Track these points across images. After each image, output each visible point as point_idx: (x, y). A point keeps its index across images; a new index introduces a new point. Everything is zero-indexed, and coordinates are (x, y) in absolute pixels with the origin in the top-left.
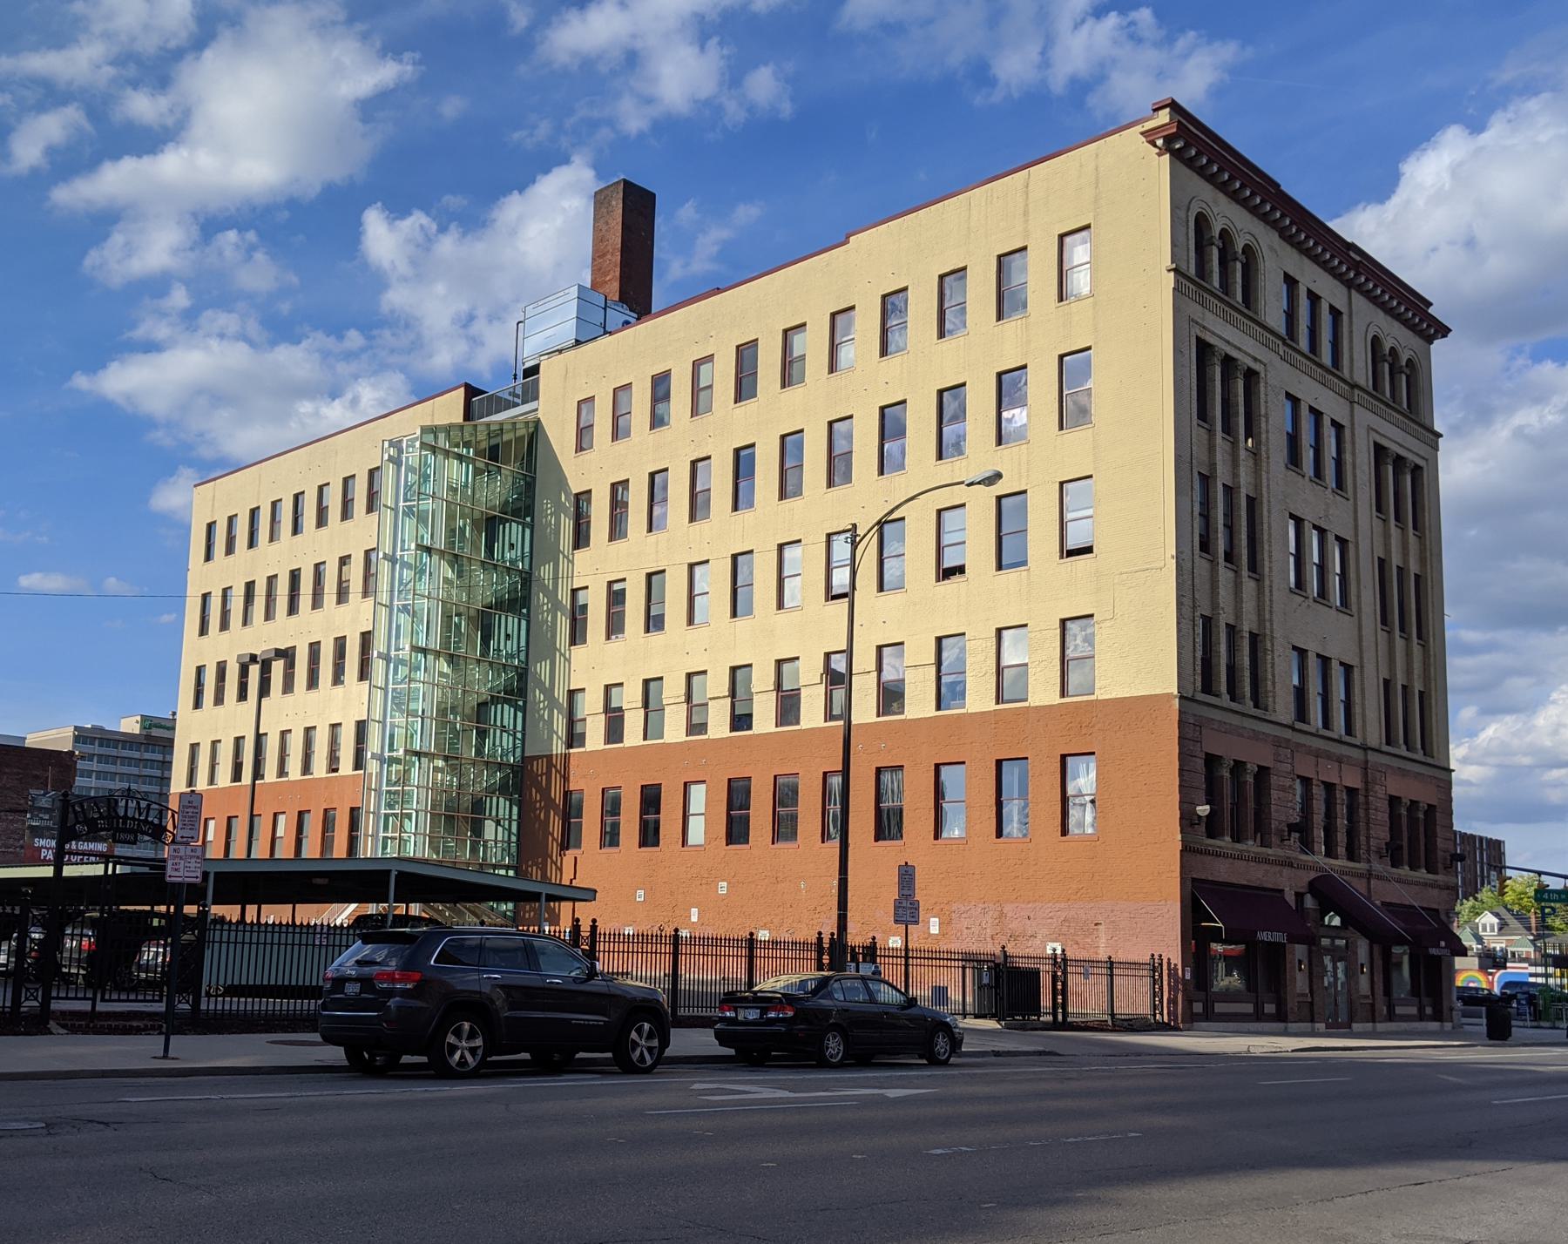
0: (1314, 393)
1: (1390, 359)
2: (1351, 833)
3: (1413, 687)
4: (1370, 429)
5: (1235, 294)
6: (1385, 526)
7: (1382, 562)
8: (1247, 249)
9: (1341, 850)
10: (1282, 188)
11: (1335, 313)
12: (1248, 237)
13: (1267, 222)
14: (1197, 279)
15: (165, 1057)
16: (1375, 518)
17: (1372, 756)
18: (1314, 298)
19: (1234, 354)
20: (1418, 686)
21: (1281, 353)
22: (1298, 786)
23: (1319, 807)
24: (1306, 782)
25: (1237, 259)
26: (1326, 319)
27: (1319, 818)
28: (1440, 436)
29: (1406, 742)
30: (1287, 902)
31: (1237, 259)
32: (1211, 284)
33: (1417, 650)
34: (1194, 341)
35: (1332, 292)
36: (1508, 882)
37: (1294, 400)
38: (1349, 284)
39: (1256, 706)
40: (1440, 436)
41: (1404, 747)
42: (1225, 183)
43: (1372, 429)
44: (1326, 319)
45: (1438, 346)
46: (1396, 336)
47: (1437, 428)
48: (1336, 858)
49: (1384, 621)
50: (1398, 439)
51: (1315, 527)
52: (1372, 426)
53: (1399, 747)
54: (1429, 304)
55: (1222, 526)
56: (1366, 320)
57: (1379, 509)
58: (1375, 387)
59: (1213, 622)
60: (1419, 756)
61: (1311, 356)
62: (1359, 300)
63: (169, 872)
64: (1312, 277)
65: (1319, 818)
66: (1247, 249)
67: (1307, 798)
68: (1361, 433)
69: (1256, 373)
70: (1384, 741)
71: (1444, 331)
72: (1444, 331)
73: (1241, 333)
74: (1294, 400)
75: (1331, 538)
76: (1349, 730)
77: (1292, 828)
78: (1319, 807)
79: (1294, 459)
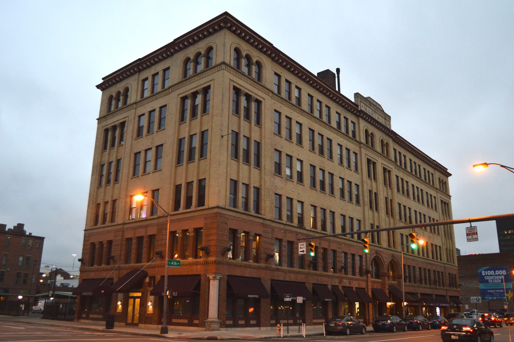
0: (401, 175)
1: (386, 145)
2: (443, 282)
3: (375, 224)
4: (440, 197)
5: (385, 153)
6: (250, 126)
7: (386, 198)
8: (372, 133)
9: (428, 283)
10: (274, 45)
11: (432, 174)
12: (372, 131)
13: (335, 102)
14: (353, 138)
15: (299, 332)
16: (368, 179)
17: (446, 265)
18: (400, 153)
19: (446, 201)
20: (451, 249)
21: (271, 96)
22: (343, 254)
23: (350, 260)
24: (346, 254)
25: (369, 136)
26: (431, 175)
27: (350, 265)
28: (451, 196)
29: (394, 246)
30: (339, 289)
31: (369, 136)
32: (369, 145)
33: (451, 242)
34: (366, 158)
35: (431, 170)
36: (103, 242)
37: (341, 146)
38: (434, 168)
39: (379, 244)
40: (451, 196)
41: (393, 248)
42: (315, 86)
43: (232, 80)
44: (431, 175)
45: (449, 178)
46: (443, 177)
47: (451, 195)
48: (427, 285)
49: (387, 214)
50: (445, 198)
51: (298, 159)
52: (231, 79)
53: (392, 248)
54: (447, 169)
55: (231, 145)
56: (437, 175)
57: (385, 184)
58: (383, 153)
59: (238, 182)
60: (377, 245)
61: (320, 119)
62: (436, 172)
63: (297, 301)
64: (399, 149)
65: (350, 265)
66: (372, 133)
67: (346, 258)
68: (439, 197)
69: (390, 171)
70: (388, 246)
71: (450, 175)
72: (450, 175)
73: (247, 84)
74: (341, 146)
75: (294, 160)
76: (441, 260)
77: (342, 267)
78: (350, 260)
79: (398, 190)
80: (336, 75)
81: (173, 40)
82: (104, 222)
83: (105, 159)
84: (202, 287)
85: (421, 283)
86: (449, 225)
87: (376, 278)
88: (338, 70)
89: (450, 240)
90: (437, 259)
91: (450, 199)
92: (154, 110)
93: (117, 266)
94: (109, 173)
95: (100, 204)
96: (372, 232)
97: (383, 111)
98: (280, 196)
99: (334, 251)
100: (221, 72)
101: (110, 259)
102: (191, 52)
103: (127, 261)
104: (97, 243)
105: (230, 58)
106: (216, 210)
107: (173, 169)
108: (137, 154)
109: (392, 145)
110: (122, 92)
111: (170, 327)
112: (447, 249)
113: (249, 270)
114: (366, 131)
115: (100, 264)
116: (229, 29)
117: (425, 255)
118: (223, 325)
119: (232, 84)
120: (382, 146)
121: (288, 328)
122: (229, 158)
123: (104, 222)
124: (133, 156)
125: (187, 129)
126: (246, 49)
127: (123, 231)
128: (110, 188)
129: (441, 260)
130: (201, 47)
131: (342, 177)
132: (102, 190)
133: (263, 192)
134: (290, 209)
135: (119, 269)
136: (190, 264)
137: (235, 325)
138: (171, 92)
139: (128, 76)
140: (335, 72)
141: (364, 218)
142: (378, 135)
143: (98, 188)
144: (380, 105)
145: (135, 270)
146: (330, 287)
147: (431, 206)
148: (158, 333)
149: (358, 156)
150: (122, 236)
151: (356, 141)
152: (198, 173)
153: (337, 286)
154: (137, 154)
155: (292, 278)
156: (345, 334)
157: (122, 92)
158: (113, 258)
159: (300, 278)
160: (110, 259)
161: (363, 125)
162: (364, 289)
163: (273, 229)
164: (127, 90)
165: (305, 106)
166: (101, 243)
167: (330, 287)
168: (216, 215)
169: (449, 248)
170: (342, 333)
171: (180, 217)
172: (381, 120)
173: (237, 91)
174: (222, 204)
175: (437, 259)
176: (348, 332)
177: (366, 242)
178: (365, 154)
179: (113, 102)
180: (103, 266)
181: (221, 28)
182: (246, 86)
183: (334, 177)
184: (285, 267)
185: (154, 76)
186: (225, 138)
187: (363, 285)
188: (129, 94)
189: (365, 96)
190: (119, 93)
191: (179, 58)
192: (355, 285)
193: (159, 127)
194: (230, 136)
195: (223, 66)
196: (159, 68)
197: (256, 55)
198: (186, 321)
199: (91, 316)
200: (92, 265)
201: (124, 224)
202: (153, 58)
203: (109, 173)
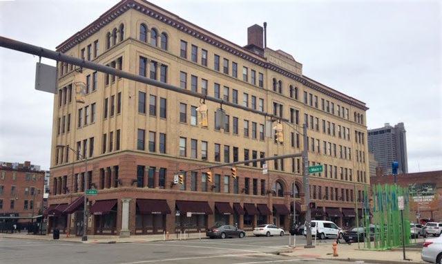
0: (310, 113)
45: (367, 111)
58: (291, 97)
76: (351, 180)
81: (98, 17)
82: (111, 150)
83: (61, 114)
84: (119, 207)
85: (343, 200)
86: (296, 158)
87: (279, 196)
88: (265, 24)
90: (346, 179)
92: (89, 75)
93: (70, 194)
94: (113, 107)
96: (276, 160)
97: (294, 61)
98: (256, 123)
99: (336, 167)
100: (128, 46)
101: (66, 190)
102: (110, 28)
103: (76, 190)
104: (105, 169)
105: (137, 34)
106: (126, 153)
108: (80, 110)
109: (301, 88)
110: (118, 28)
111: (88, 236)
112: (358, 171)
113: (155, 194)
114: (274, 80)
115: (109, 187)
116: (135, 8)
117: (333, 177)
118: (134, 233)
119: (138, 55)
120: (291, 91)
122: (137, 113)
123: (111, 150)
124: (78, 111)
125: (109, 91)
126: (151, 23)
127: (73, 169)
128: (113, 119)
129: (351, 180)
130: (116, 24)
131: (247, 119)
132: (60, 137)
133: (168, 137)
134: (195, 148)
135: (72, 197)
136: (112, 192)
137: (144, 233)
138: (60, 79)
139: (122, 13)
140: (262, 26)
142: (287, 82)
143: (57, 136)
144: (288, 58)
145: (80, 196)
146: (232, 205)
149: (265, 102)
150: (73, 172)
151: (263, 89)
152: (116, 125)
153: (239, 203)
154: (80, 110)
155: (196, 198)
156: (221, 238)
157: (118, 28)
158: (94, 184)
159: (203, 199)
160: (66, 190)
162: (266, 205)
163: (178, 164)
164: (122, 26)
165: (211, 65)
166: (109, 168)
167: (232, 205)
168: (126, 156)
170: (220, 237)
171: (105, 158)
172: (291, 69)
173: (144, 60)
174: (131, 148)
175: (346, 179)
177: (234, 171)
178: (271, 99)
179: (111, 39)
180: (62, 195)
181: (128, 8)
182: (151, 54)
183: (239, 121)
184: (189, 191)
186: (133, 98)
187: (265, 202)
188: (124, 30)
189: (275, 50)
190: (115, 29)
192: (256, 202)
193: (94, 89)
194: (137, 96)
195: (130, 41)
196: (91, 40)
197: (161, 27)
198: (110, 232)
199: (104, 232)
200: (103, 188)
201: (73, 163)
202: (116, 11)
203: (113, 107)
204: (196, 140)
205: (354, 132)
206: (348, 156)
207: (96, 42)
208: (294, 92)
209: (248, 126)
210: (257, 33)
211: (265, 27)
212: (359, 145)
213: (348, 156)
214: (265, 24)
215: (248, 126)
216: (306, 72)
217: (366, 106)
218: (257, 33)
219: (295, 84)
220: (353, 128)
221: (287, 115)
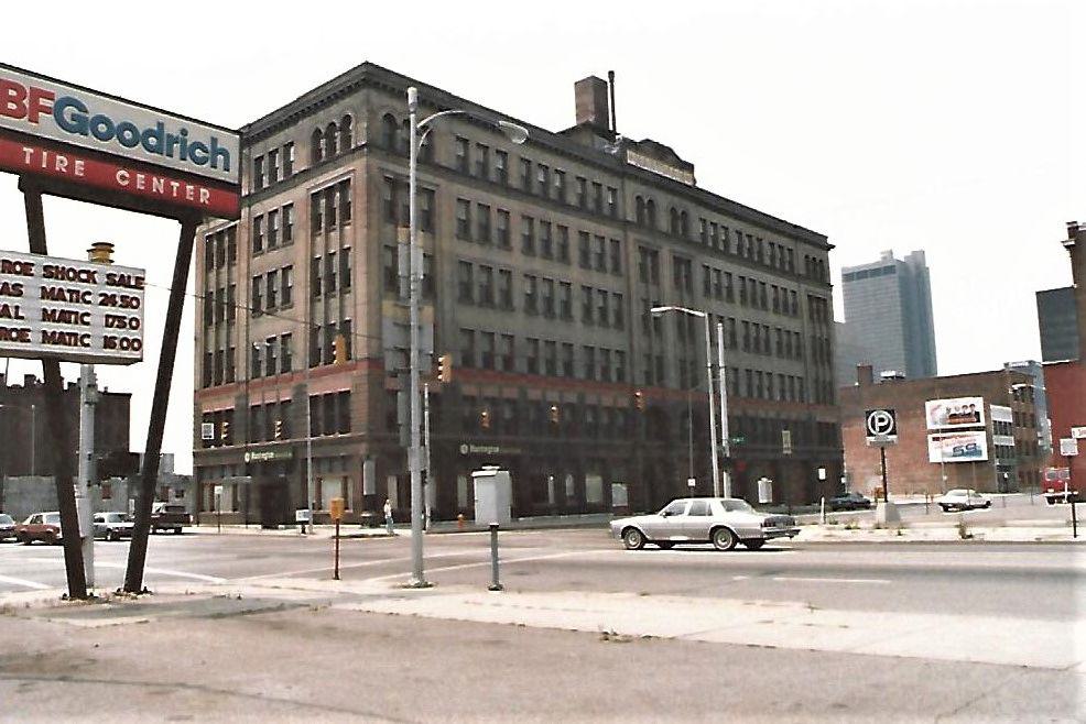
45: (831, 253)
46: (815, 253)
50: (819, 292)
56: (802, 250)
80: (609, 84)
88: (611, 74)
89: (826, 363)
91: (831, 290)
95: (223, 289)
102: (321, 120)
107: (95, 607)
112: (816, 381)
121: (1073, 506)
138: (325, 163)
141: (631, 346)
144: (663, 152)
147: (786, 307)
148: (954, 534)
161: (632, 189)
169: (821, 379)
176: (109, 538)
185: (272, 154)
191: (306, 124)
204: (532, 219)
205: (804, 299)
206: (797, 395)
207: (347, 119)
208: (680, 224)
209: (603, 250)
210: (596, 94)
211: (612, 81)
212: (817, 325)
213: (797, 395)
214: (611, 74)
215: (603, 250)
216: (706, 180)
217: (830, 241)
218: (596, 94)
219: (682, 204)
220: (803, 290)
221: (664, 223)
